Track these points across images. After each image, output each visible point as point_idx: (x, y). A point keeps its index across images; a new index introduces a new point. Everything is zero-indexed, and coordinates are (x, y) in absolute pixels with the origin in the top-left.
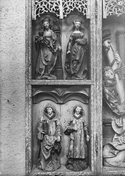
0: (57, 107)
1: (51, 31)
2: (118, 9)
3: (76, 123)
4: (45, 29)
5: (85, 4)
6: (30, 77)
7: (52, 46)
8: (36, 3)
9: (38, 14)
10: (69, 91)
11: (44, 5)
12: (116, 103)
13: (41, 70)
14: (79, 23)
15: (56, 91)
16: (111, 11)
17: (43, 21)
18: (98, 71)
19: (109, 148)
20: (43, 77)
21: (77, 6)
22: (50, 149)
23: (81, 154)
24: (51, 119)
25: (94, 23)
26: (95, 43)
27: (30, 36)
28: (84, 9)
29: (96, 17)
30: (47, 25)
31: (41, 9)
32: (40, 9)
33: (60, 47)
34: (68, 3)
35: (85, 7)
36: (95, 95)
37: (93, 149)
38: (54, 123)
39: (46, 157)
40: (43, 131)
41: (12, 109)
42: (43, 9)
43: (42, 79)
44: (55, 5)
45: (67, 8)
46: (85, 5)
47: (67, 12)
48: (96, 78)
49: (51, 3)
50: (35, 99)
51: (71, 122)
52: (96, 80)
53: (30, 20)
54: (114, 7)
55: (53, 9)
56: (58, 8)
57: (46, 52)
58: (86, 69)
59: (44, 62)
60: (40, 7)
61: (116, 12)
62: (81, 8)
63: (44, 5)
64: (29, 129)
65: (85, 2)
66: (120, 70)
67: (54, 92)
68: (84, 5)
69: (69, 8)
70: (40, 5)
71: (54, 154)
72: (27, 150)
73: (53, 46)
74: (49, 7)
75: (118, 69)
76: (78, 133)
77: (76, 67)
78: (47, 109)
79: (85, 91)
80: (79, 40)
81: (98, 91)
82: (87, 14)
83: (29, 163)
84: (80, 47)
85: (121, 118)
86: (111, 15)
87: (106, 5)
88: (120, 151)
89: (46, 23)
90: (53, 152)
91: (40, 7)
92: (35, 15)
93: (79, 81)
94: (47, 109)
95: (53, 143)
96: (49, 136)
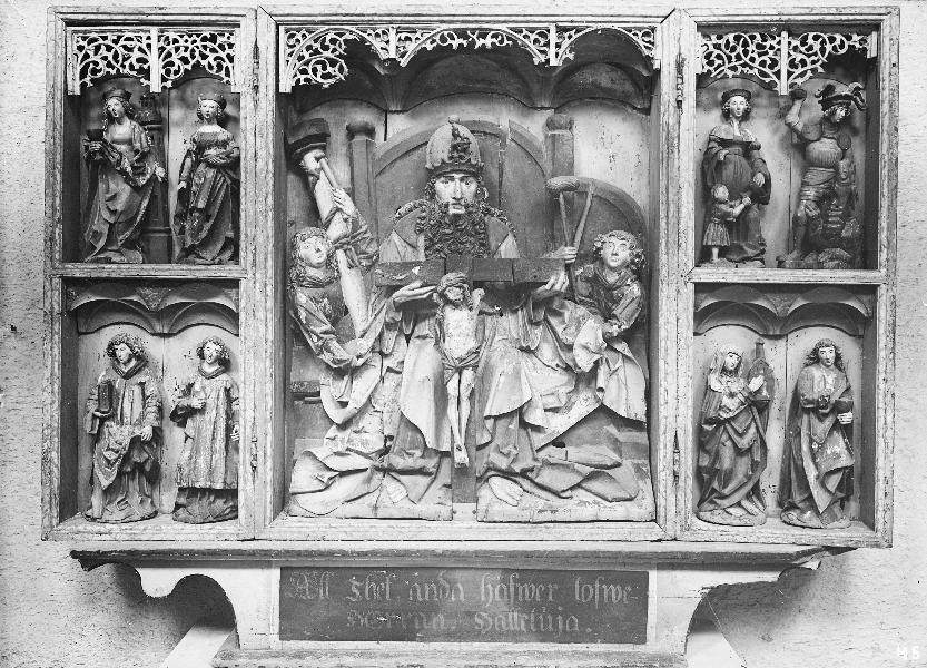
0: (155, 348)
1: (134, 123)
2: (324, 68)
3: (203, 388)
4: (112, 120)
5: (228, 51)
6: (57, 256)
7: (129, 169)
8: (81, 48)
9: (87, 80)
10: (182, 296)
11: (106, 54)
12: (325, 332)
13: (97, 235)
14: (215, 104)
15: (141, 295)
16: (304, 72)
17: (105, 97)
18: (260, 239)
19: (311, 467)
20: (102, 256)
21: (204, 57)
22: (116, 460)
23: (211, 471)
24: (127, 376)
25: (251, 105)
26: (253, 163)
27: (58, 141)
28: (224, 65)
29: (256, 88)
30: (117, 108)
31: (96, 64)
32: (92, 66)
33: (160, 172)
34: (177, 49)
35: (226, 59)
36: (250, 307)
37: (244, 461)
38: (137, 390)
39: (106, 483)
40: (97, 410)
41: (26, 353)
42: (102, 64)
43: (97, 261)
44: (136, 54)
45: (172, 64)
46: (228, 55)
47: (172, 75)
48: (254, 261)
49: (125, 47)
50: (77, 322)
51: (190, 386)
52: (254, 264)
53: (59, 95)
54: (313, 61)
55: (131, 65)
56: (146, 61)
57: (112, 186)
58: (230, 234)
59: (106, 215)
60: (93, 58)
61: (319, 74)
62: (214, 64)
63: (106, 54)
64: (53, 402)
65: (226, 47)
66: (353, 238)
67: (134, 298)
68: (223, 55)
69: (177, 62)
70: (91, 53)
71: (132, 475)
72: (45, 460)
73: (133, 168)
74: (120, 58)
75: (345, 236)
76: (208, 419)
77: (200, 228)
78: (116, 347)
79: (227, 296)
80: (212, 152)
81: (259, 297)
82: (231, 80)
83: (51, 498)
84: (211, 173)
85: (346, 378)
86: (302, 82)
87: (291, 54)
88: (343, 474)
89: (114, 105)
90: (129, 469)
91: (93, 58)
92: (78, 83)
93: (203, 267)
94: (116, 347)
95: (127, 442)
96: (117, 424)
